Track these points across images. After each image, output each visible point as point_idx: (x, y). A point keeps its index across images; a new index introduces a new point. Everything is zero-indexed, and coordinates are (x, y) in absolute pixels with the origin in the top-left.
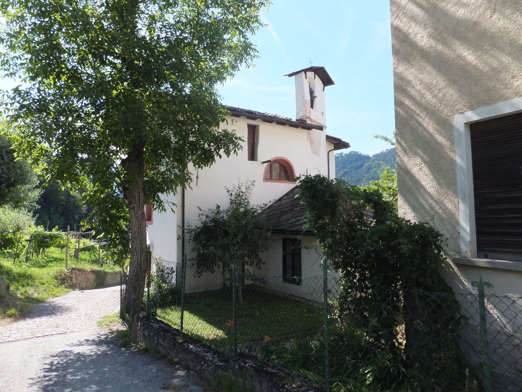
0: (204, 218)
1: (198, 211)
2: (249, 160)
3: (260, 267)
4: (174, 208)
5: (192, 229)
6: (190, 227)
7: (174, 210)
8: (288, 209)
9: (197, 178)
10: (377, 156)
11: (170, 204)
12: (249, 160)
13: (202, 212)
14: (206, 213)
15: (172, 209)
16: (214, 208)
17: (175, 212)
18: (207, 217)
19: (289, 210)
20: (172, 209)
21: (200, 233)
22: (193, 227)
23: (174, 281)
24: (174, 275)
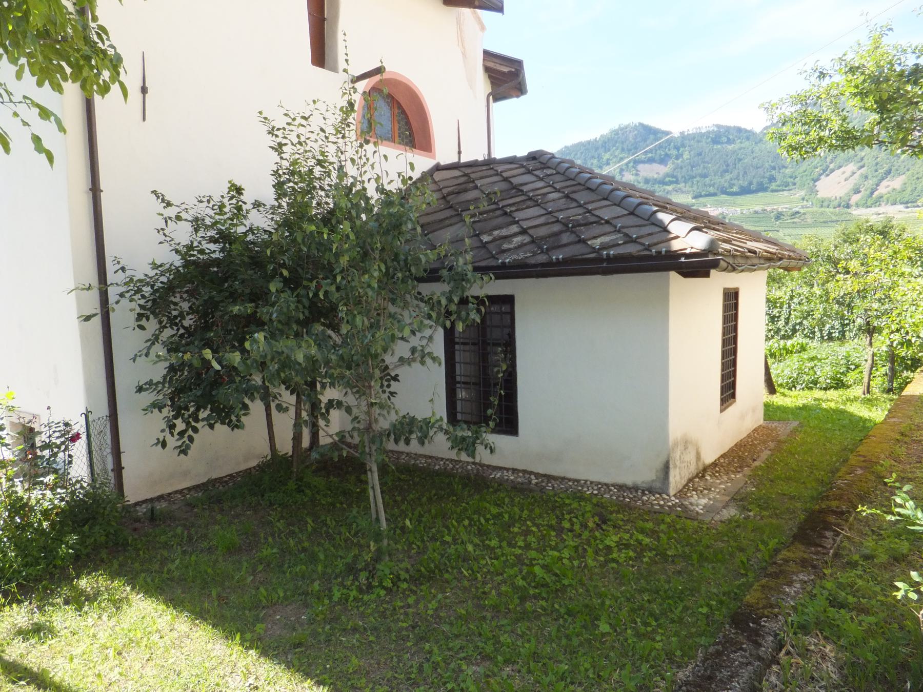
0: (183, 234)
1: (159, 207)
2: (725, 289)
3: (392, 389)
4: (47, 131)
5: (139, 276)
6: (128, 273)
7: (46, 145)
8: (442, 217)
9: (144, 90)
10: (683, 136)
11: (22, 109)
12: (725, 289)
13: (171, 212)
14: (191, 212)
15: (37, 140)
16: (219, 191)
17: (50, 158)
18: (197, 223)
19: (447, 218)
20: (37, 140)
21: (170, 288)
22: (141, 269)
23: (79, 470)
24: (79, 449)
